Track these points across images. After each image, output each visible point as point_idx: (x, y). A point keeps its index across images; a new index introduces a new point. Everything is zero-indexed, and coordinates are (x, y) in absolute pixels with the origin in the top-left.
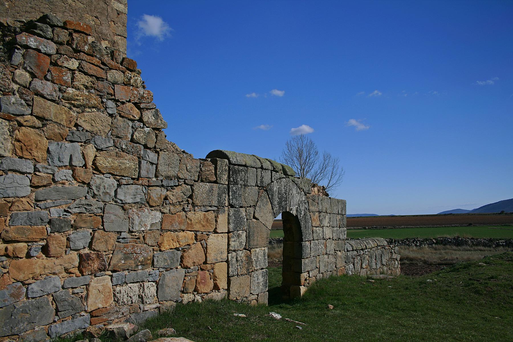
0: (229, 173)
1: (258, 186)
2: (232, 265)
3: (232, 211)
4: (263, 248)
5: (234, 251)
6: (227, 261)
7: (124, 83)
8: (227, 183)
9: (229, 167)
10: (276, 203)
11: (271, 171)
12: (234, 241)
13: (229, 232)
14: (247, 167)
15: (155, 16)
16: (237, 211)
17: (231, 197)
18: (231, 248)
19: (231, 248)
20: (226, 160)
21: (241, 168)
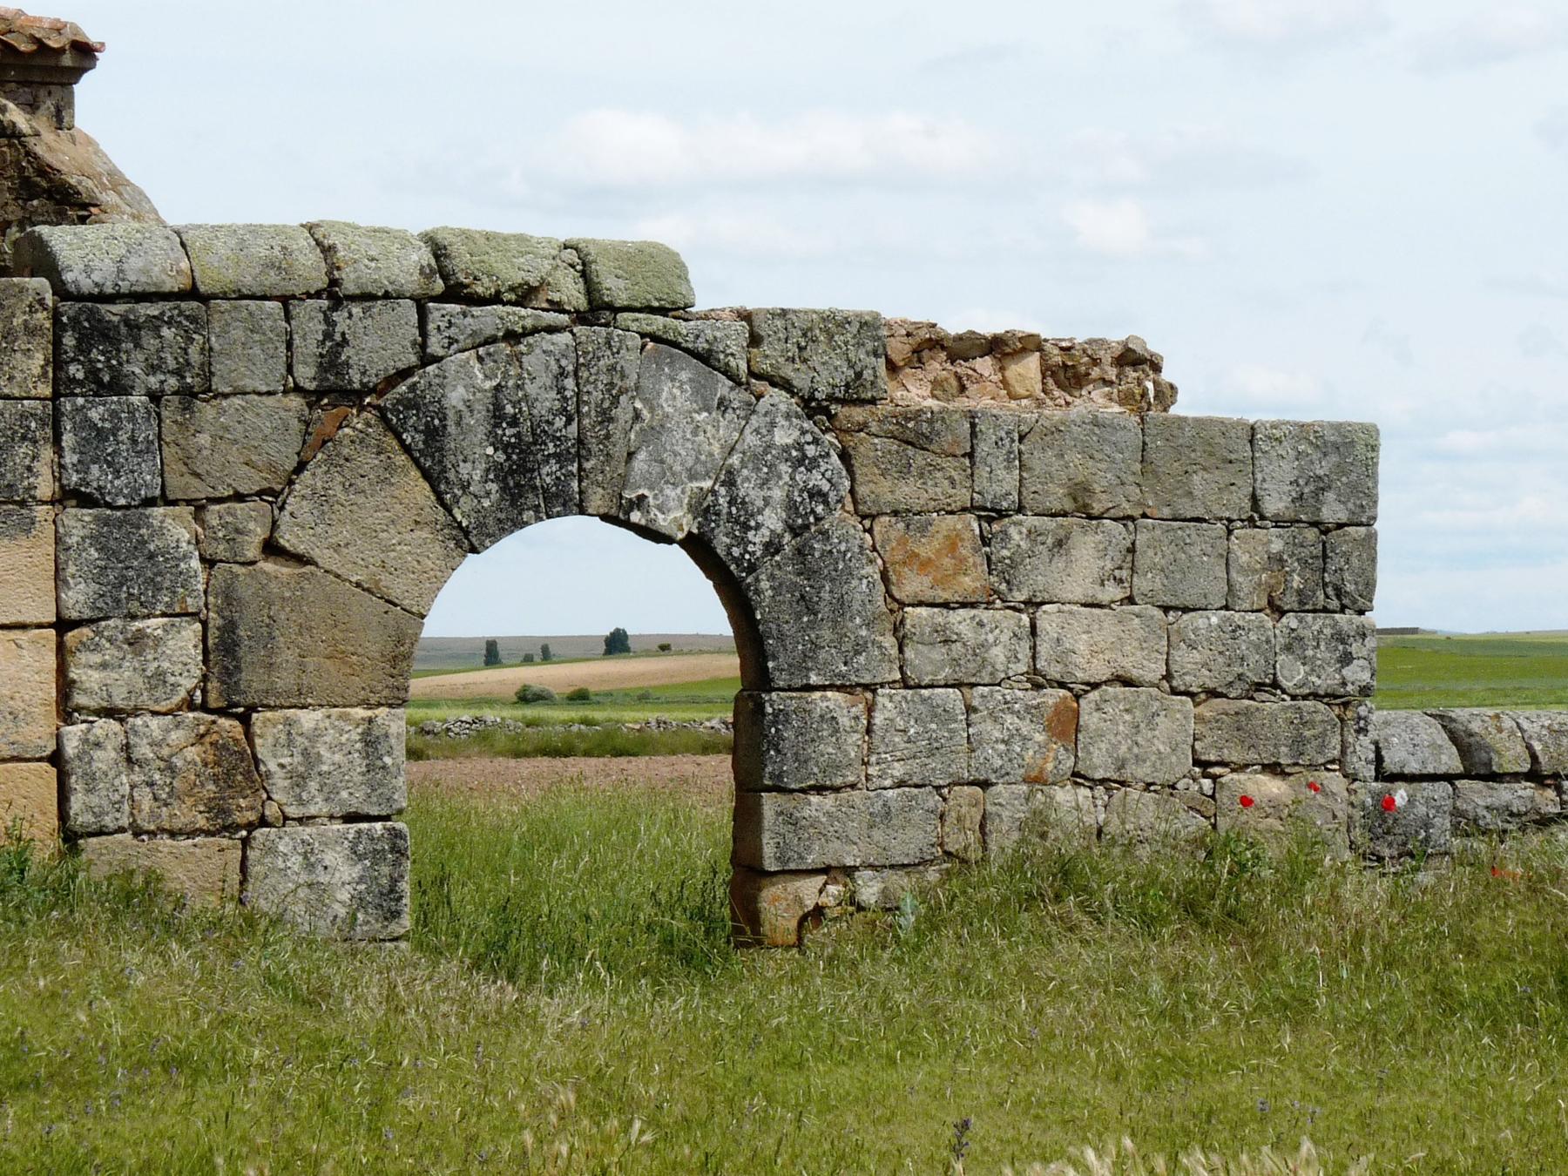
0: (57, 343)
1: (298, 389)
2: (91, 779)
3: (79, 522)
4: (360, 712)
5: (110, 712)
6: (56, 758)
7: (196, 1073)
8: (47, 391)
9: (56, 316)
10: (472, 472)
11: (421, 303)
12: (104, 666)
13: (63, 625)
14: (205, 299)
15: (729, 617)
16: (120, 524)
17: (70, 458)
18: (80, 699)
19: (80, 699)
20: (41, 283)
21: (153, 310)
